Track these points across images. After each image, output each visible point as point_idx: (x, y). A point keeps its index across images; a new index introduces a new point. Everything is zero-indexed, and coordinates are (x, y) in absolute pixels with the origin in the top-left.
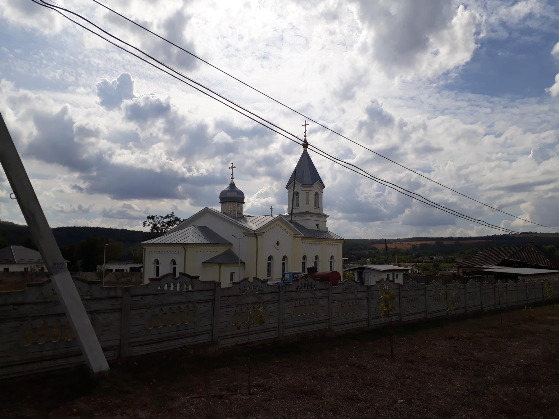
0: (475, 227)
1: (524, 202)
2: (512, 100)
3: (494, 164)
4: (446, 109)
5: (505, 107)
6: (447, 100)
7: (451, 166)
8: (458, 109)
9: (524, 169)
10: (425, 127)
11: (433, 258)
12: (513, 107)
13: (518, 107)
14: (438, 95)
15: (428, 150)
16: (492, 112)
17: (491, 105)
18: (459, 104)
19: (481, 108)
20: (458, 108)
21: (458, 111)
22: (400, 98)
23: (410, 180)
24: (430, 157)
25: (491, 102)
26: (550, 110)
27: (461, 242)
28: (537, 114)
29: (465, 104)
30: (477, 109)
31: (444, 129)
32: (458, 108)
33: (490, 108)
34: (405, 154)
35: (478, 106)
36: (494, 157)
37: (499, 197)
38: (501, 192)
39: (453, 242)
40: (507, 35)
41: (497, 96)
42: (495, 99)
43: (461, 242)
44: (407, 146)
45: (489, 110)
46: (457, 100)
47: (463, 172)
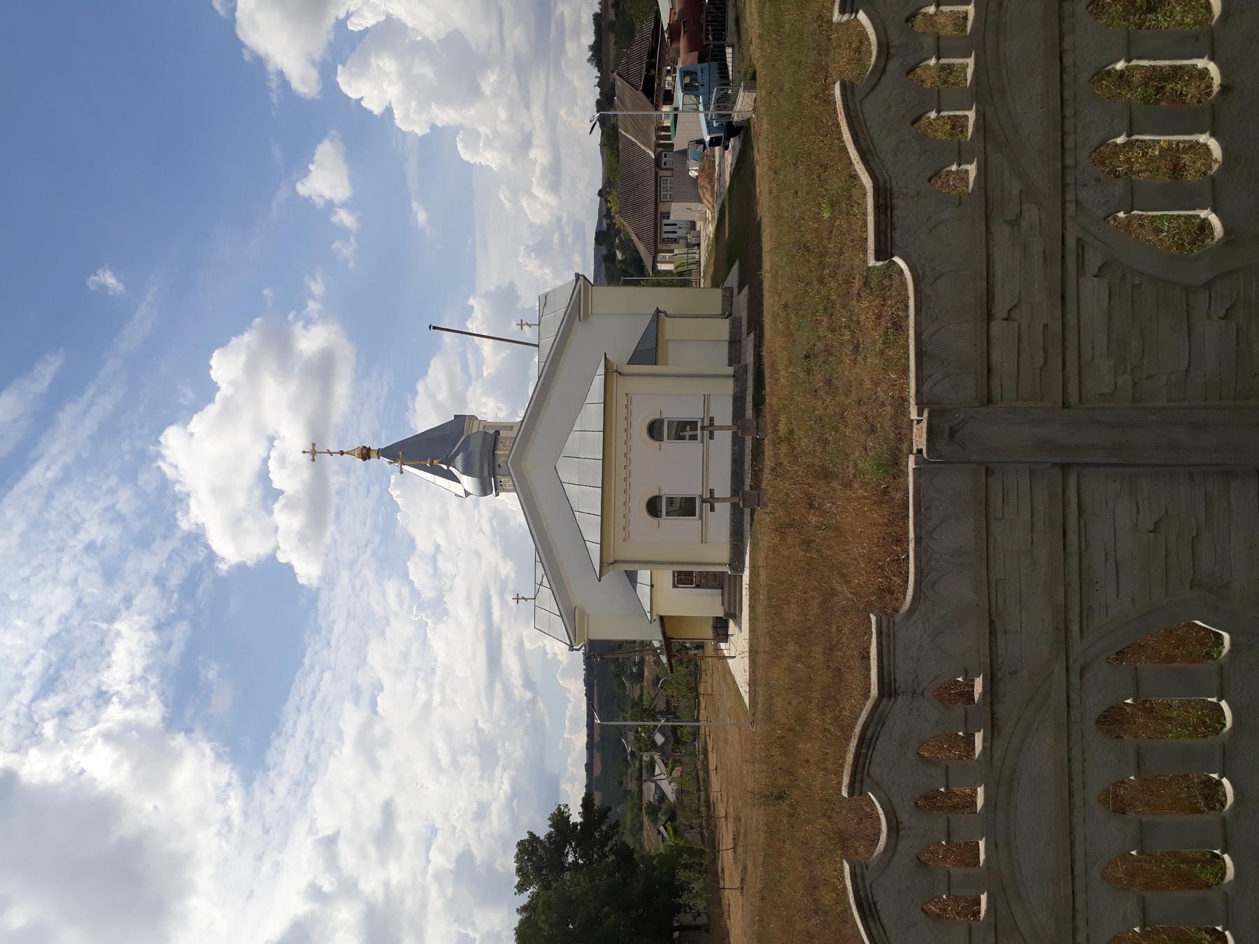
0: (566, 736)
1: (521, 644)
2: (318, 630)
3: (437, 698)
4: (307, 757)
5: (328, 642)
6: (288, 758)
7: (532, 266)
8: (312, 734)
9: (455, 644)
10: (330, 843)
11: (633, 753)
12: (330, 630)
13: (334, 621)
14: (272, 774)
15: (385, 835)
16: (333, 670)
17: (317, 669)
18: (300, 732)
19: (319, 689)
20: (310, 733)
21: (316, 735)
22: (260, 858)
23: (451, 871)
24: (401, 826)
25: (312, 668)
26: (351, 569)
27: (597, 739)
28: (354, 589)
29: (304, 719)
30: (319, 697)
31: (341, 793)
32: (310, 733)
33: (323, 671)
34: (387, 885)
35: (314, 694)
36: (422, 696)
37: (507, 691)
38: (498, 686)
39: (597, 756)
40: (185, 623)
41: (304, 656)
42: (307, 662)
43: (597, 739)
44: (370, 884)
45: (327, 676)
46: (293, 735)
47: (445, 758)
